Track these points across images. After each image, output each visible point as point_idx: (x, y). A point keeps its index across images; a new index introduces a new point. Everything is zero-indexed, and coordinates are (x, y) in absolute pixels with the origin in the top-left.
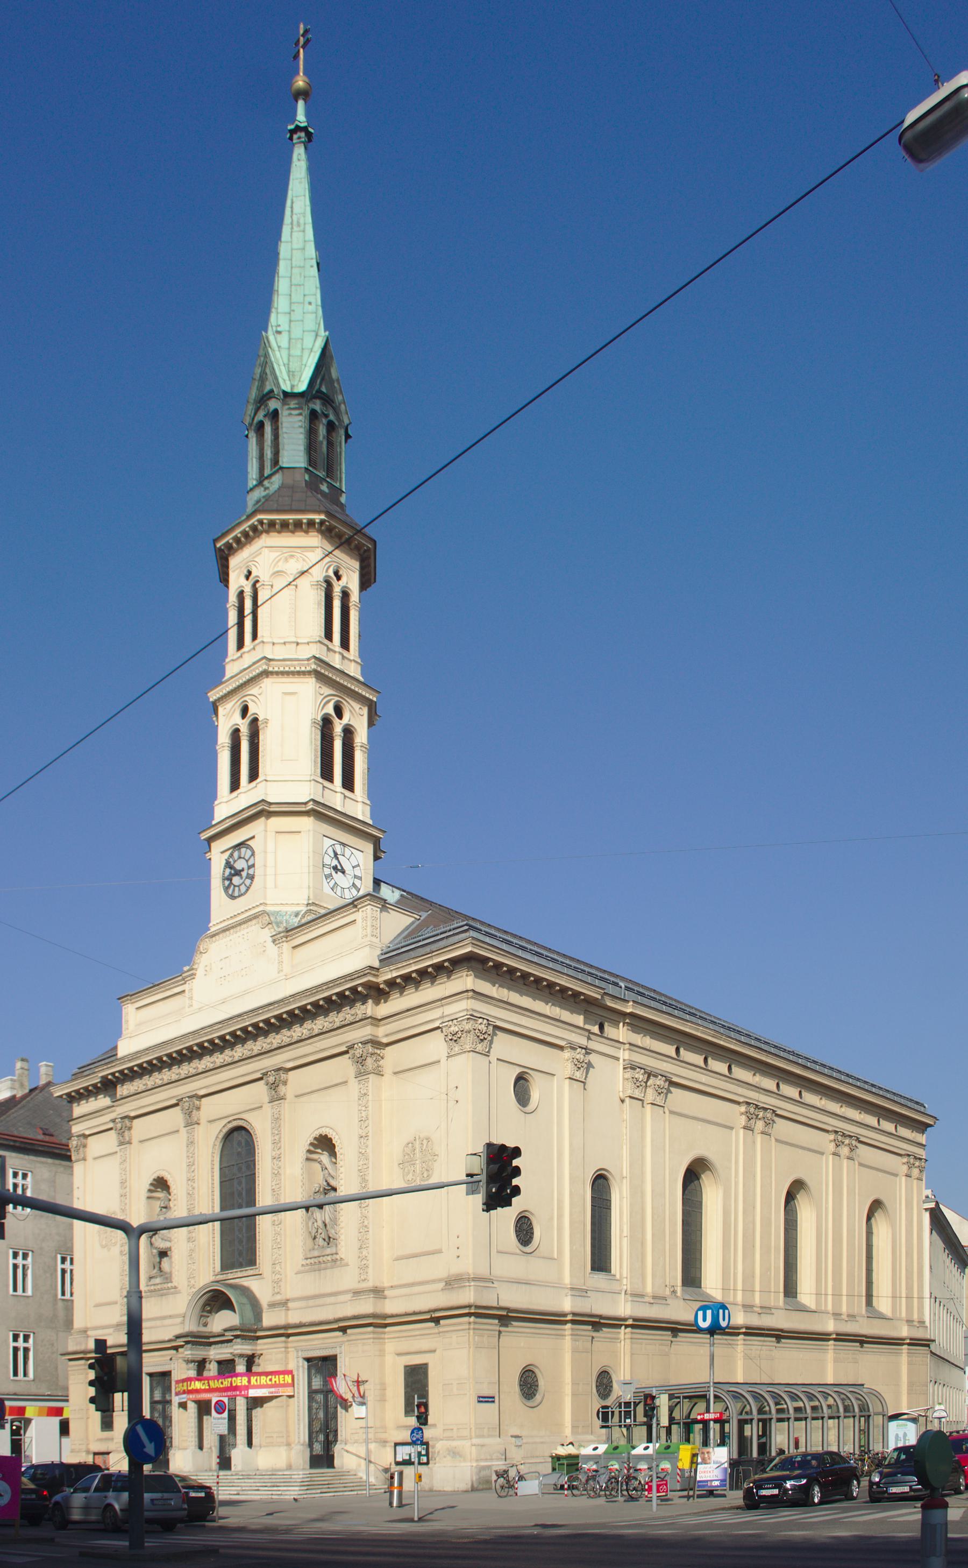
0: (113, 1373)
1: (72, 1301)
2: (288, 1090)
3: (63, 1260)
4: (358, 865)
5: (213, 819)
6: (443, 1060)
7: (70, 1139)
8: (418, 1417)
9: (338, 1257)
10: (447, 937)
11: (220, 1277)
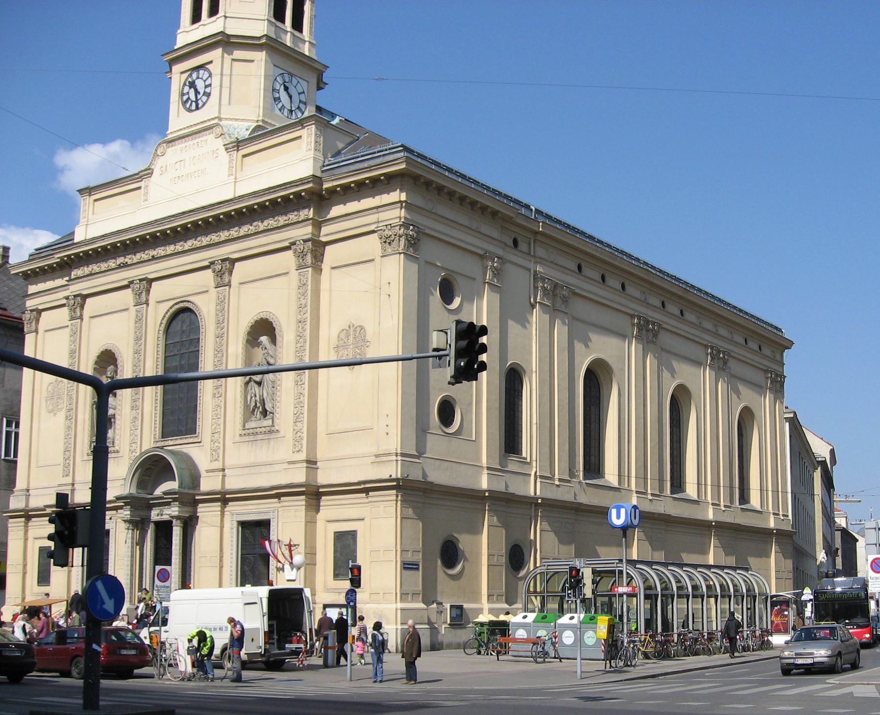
0: (75, 528)
1: (16, 462)
2: (235, 278)
3: (9, 424)
4: (299, 94)
5: (175, 44)
6: (378, 259)
7: (24, 313)
8: (352, 581)
9: (273, 428)
10: (384, 155)
11: (159, 445)
